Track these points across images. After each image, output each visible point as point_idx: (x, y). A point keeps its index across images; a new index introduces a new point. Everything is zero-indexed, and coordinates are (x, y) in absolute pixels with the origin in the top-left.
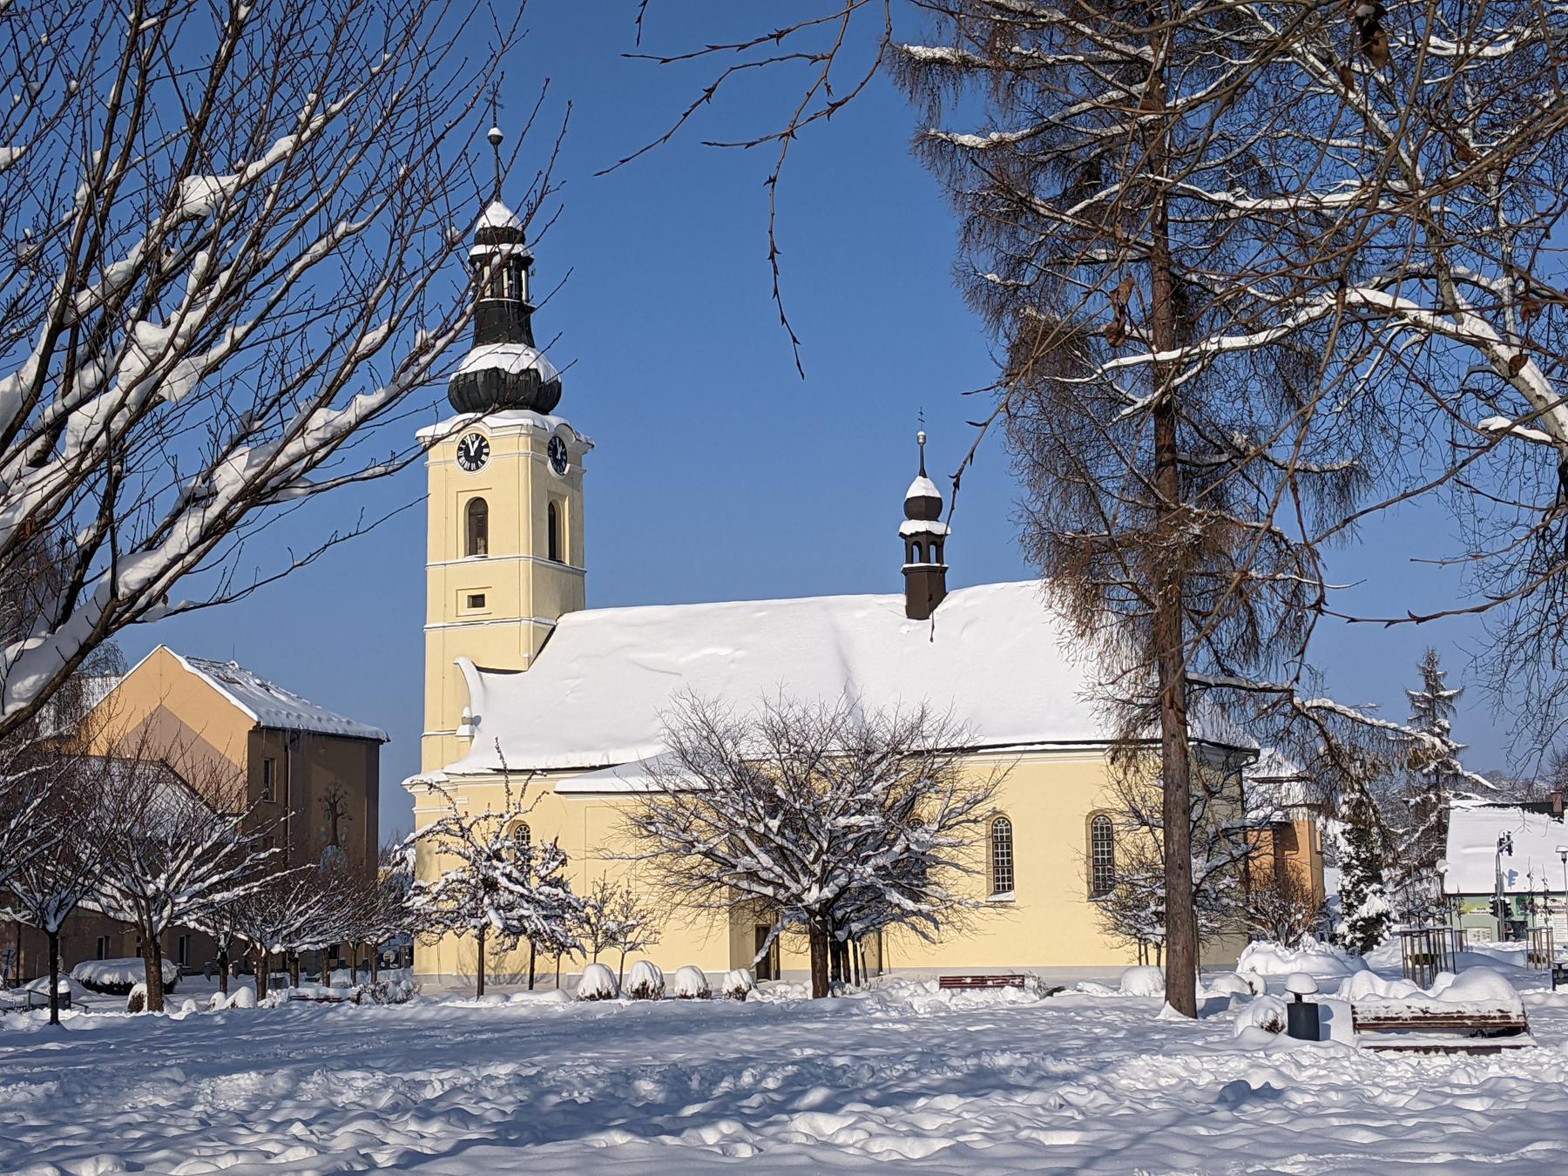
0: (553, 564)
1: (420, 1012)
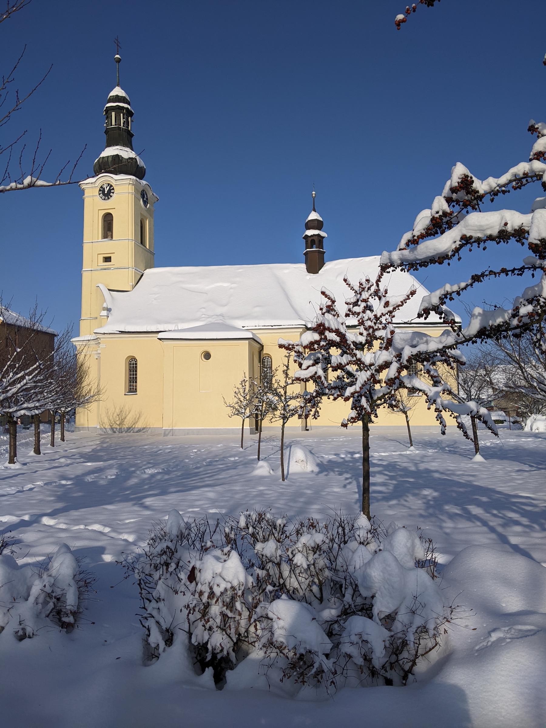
1: (410, 467)
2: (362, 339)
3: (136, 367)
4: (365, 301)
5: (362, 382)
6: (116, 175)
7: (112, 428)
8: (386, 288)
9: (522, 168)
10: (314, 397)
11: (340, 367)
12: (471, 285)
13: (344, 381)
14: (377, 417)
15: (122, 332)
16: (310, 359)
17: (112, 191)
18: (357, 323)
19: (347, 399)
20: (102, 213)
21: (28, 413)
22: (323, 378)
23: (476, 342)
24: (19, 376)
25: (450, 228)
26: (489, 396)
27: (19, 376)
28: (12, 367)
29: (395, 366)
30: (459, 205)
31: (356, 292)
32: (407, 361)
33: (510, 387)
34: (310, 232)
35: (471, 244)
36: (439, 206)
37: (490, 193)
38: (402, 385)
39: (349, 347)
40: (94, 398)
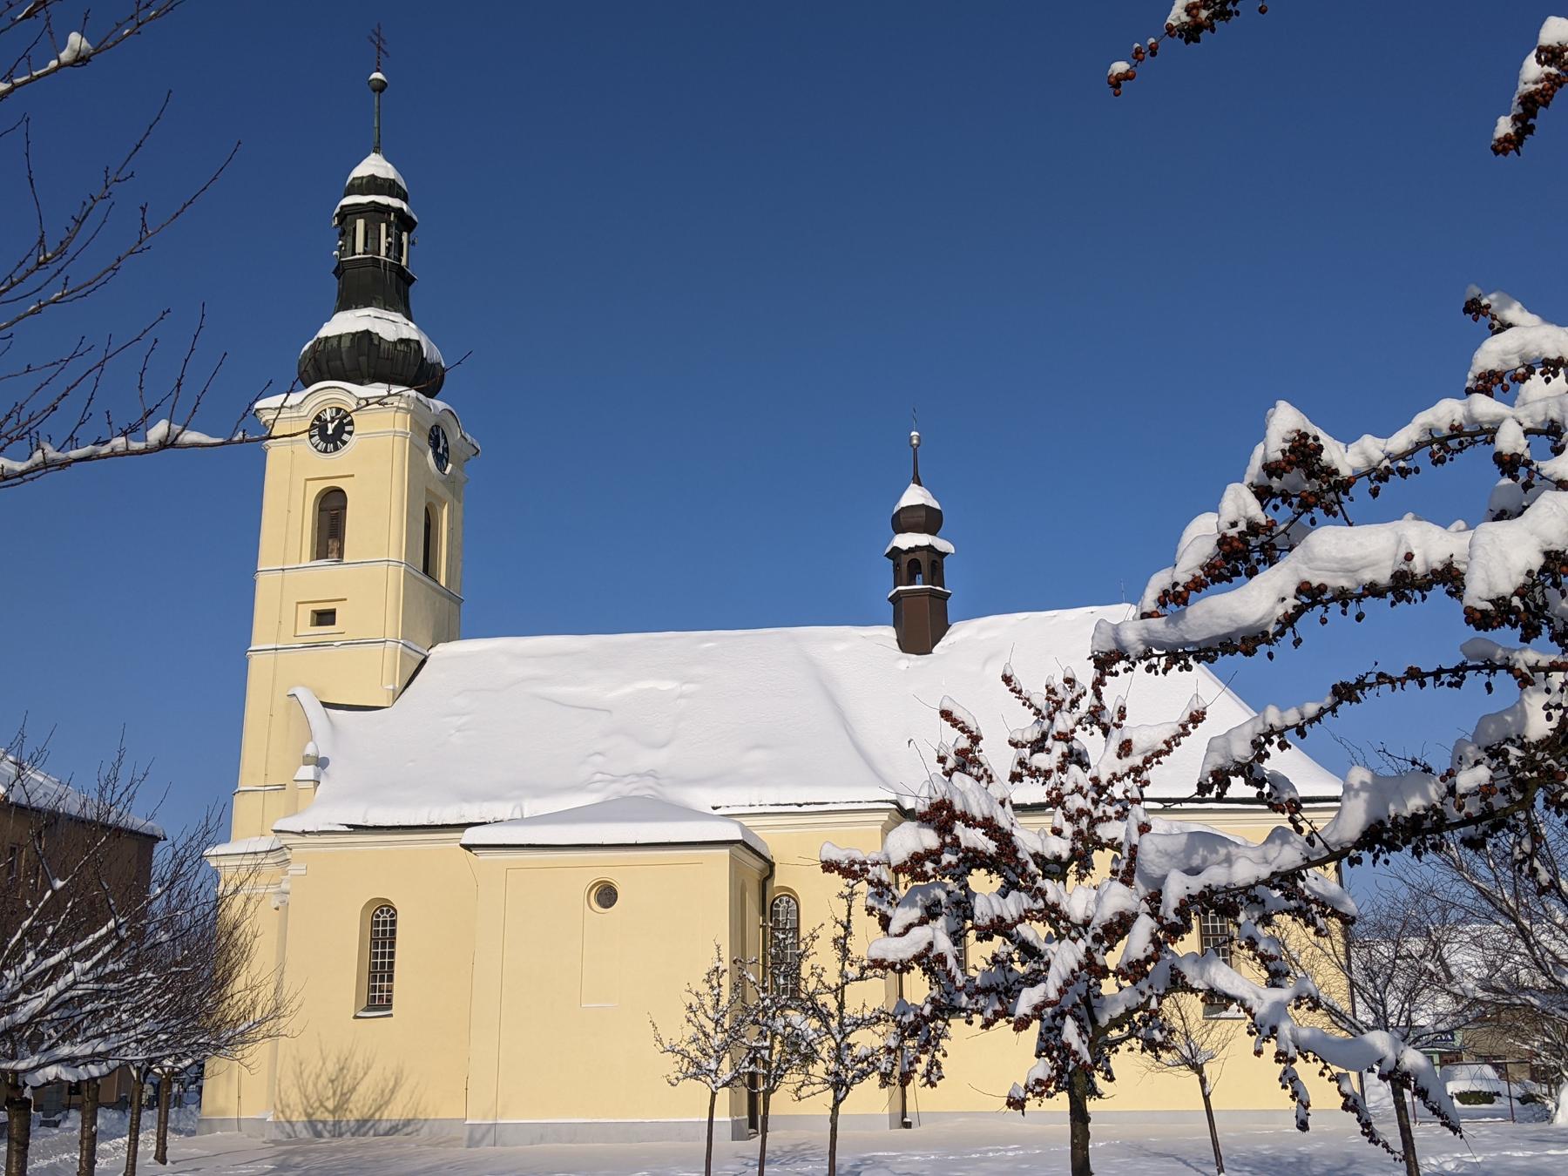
0: (426, 579)
2: (1061, 847)
3: (393, 932)
4: (1065, 737)
5: (1065, 974)
6: (361, 384)
7: (310, 1122)
8: (1120, 703)
9: (1447, 412)
10: (927, 1020)
11: (999, 927)
12: (1333, 709)
13: (1011, 970)
14: (1112, 1079)
15: (357, 829)
16: (913, 904)
17: (348, 428)
18: (1044, 799)
19: (1022, 1024)
20: (316, 488)
21: (67, 1075)
22: (951, 962)
23: (1359, 861)
24: (53, 960)
25: (1272, 561)
26: (1439, 1017)
27: (53, 960)
28: (33, 934)
29: (1143, 928)
30: (1291, 505)
31: (1038, 712)
32: (1177, 912)
33: (1497, 990)
34: (905, 541)
35: (1325, 604)
36: (1238, 508)
37: (1368, 474)
38: (1177, 982)
39: (1024, 870)
40: (264, 1028)
